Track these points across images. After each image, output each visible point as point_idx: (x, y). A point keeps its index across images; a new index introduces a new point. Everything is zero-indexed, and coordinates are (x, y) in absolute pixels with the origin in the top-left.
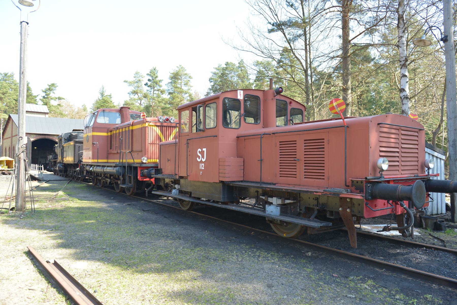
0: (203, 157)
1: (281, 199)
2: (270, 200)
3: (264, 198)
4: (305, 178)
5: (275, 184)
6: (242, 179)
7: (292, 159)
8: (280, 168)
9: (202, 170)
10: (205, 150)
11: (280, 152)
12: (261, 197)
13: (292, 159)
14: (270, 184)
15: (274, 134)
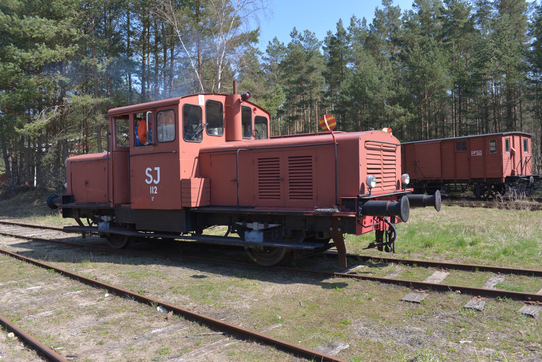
0: (155, 178)
1: (262, 223)
2: (249, 225)
3: (241, 224)
4: (290, 198)
5: (254, 207)
6: (208, 204)
7: (276, 178)
8: (260, 189)
9: (154, 195)
10: (157, 169)
11: (259, 171)
12: (237, 223)
13: (276, 178)
14: (247, 207)
15: (251, 150)
